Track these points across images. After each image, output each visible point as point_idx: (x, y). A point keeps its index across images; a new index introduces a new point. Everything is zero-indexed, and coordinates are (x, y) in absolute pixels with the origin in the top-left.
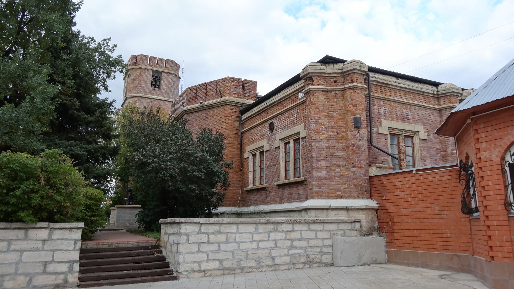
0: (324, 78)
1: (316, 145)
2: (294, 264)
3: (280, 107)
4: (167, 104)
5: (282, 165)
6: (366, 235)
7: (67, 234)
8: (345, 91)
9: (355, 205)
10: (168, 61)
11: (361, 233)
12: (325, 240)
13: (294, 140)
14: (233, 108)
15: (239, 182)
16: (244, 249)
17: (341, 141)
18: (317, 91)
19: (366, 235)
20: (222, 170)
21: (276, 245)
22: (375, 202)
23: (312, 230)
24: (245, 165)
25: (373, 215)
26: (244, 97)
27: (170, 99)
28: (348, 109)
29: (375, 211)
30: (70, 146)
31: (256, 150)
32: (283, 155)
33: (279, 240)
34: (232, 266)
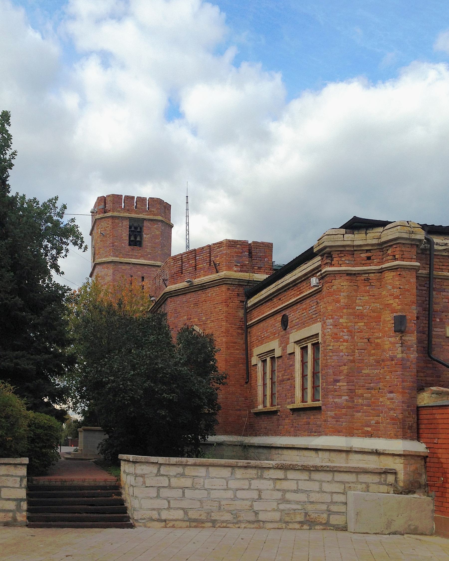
0: (351, 253)
1: (334, 357)
2: (287, 523)
3: (296, 292)
4: (153, 271)
5: (297, 381)
6: (403, 493)
7: (12, 471)
8: (383, 273)
9: (389, 449)
10: (152, 200)
11: (395, 489)
12: (334, 495)
13: (313, 344)
14: (234, 288)
15: (245, 399)
16: (216, 498)
17: (373, 352)
18: (337, 275)
19: (403, 493)
20: (207, 389)
21: (260, 496)
22: (424, 446)
23: (315, 481)
24: (253, 375)
25: (418, 465)
26: (252, 269)
27: (158, 262)
28: (387, 302)
29: (422, 459)
30: (16, 359)
31: (266, 355)
32: (299, 366)
33: (264, 490)
34: (200, 518)
